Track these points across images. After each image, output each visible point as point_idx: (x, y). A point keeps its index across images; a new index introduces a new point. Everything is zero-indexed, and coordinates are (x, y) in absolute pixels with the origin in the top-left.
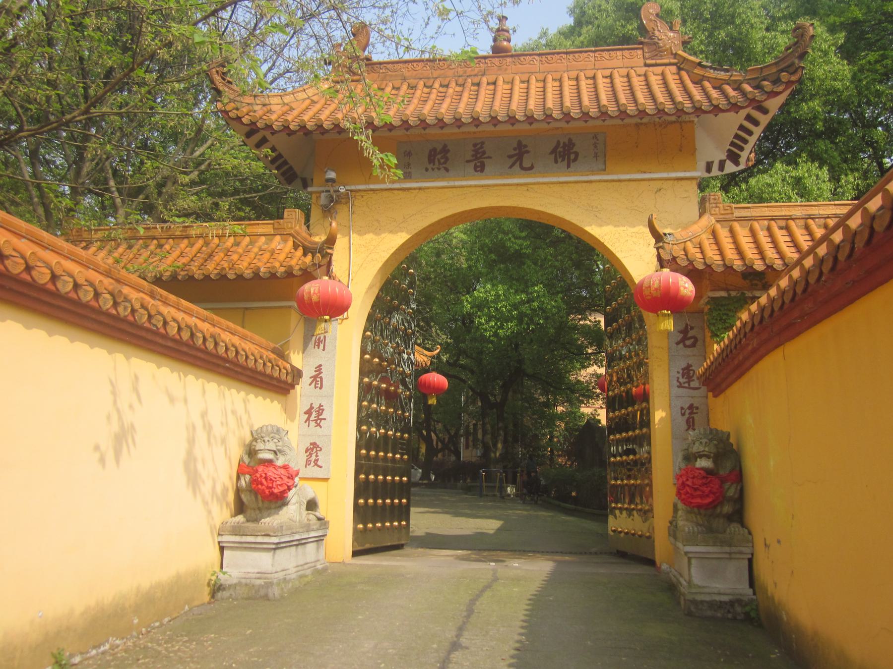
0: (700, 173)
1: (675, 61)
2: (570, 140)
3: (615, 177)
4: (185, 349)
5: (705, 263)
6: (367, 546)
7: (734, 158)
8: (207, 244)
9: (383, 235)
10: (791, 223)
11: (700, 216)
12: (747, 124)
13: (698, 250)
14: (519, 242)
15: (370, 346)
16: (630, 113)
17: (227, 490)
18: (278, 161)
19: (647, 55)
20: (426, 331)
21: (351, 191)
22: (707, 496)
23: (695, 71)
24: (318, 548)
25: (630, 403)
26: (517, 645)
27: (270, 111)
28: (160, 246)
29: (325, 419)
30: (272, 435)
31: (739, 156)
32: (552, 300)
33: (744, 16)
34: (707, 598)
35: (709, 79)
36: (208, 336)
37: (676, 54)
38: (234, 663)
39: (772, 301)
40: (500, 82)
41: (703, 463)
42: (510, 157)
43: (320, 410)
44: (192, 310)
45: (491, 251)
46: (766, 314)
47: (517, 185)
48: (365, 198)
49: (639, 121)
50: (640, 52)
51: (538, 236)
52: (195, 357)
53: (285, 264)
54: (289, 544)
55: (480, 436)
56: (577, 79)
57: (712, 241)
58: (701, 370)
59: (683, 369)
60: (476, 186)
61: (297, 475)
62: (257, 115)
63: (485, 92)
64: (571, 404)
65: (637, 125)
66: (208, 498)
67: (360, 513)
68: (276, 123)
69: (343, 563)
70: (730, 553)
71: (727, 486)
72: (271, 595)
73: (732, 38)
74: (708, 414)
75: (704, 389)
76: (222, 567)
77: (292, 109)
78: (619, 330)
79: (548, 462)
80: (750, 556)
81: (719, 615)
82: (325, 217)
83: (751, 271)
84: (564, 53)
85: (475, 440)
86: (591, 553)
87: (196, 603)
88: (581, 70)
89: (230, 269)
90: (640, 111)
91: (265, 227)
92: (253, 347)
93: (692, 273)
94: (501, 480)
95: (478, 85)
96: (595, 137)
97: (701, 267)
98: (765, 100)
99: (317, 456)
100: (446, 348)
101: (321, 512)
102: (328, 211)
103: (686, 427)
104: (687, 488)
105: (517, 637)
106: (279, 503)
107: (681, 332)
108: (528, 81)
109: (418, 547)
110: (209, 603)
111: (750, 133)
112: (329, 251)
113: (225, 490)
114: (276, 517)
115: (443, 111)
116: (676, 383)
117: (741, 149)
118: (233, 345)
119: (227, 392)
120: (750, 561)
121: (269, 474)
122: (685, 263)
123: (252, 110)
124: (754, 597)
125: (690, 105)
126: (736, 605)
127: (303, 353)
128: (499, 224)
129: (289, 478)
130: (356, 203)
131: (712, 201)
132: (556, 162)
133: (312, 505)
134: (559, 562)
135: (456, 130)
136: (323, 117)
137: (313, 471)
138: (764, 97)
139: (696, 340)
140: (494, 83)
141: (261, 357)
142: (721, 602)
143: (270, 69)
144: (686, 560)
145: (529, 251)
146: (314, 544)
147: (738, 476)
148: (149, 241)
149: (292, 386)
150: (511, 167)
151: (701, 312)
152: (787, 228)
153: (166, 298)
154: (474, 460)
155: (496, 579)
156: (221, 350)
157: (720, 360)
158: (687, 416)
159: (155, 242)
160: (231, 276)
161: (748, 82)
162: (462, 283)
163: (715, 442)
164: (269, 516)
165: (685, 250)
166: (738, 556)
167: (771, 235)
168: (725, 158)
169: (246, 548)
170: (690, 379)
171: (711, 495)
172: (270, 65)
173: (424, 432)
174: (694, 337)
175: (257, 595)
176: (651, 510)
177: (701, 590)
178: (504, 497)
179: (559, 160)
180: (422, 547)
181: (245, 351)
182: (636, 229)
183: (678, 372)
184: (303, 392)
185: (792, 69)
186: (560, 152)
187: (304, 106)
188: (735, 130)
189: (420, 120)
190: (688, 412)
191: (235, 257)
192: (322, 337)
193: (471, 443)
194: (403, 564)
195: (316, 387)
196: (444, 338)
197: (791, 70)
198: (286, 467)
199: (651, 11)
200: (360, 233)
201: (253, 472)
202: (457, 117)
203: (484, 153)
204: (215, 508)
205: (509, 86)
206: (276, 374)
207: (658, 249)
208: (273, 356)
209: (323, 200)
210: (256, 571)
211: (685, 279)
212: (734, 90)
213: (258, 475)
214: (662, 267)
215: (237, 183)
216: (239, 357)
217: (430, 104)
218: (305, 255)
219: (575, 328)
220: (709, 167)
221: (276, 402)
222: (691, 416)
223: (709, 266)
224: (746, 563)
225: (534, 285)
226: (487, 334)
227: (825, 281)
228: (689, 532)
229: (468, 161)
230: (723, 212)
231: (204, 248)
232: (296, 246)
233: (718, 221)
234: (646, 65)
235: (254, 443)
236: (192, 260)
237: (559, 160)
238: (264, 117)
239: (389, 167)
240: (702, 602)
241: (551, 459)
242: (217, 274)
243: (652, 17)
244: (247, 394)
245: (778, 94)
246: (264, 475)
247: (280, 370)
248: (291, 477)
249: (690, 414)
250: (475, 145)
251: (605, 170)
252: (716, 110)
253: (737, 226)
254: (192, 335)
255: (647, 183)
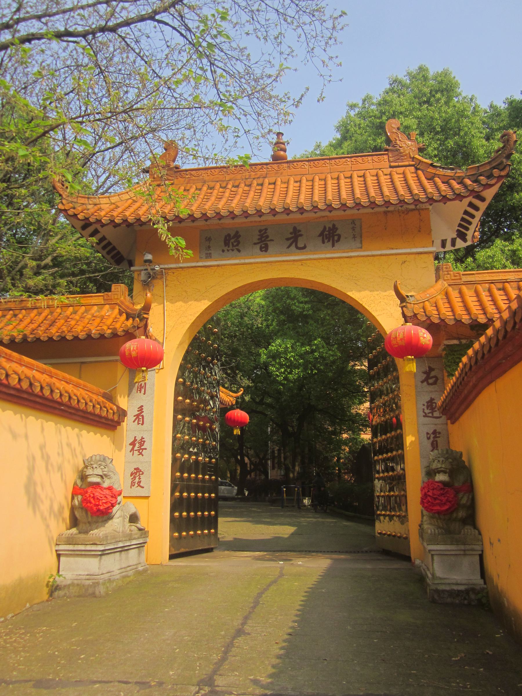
0: (436, 248)
1: (413, 163)
2: (334, 225)
3: (369, 253)
4: (25, 396)
5: (440, 318)
6: (183, 550)
7: (462, 236)
8: (51, 313)
9: (190, 303)
10: (507, 285)
11: (436, 282)
12: (470, 210)
13: (435, 308)
14: (301, 305)
15: (183, 390)
16: (378, 203)
17: (63, 508)
18: (106, 246)
19: (391, 159)
20: (232, 377)
21: (165, 269)
22: (445, 504)
23: (429, 170)
24: (139, 554)
25: (390, 429)
26: (290, 631)
27: (100, 209)
28: (15, 315)
29: (146, 449)
30: (100, 463)
31: (466, 235)
32: (329, 350)
33: (466, 129)
34: (447, 588)
35: (439, 176)
36: (44, 385)
37: (414, 158)
38: (57, 651)
39: (483, 346)
40: (279, 183)
41: (441, 477)
42: (288, 239)
43: (142, 442)
44: (33, 365)
45: (282, 312)
46: (480, 356)
47: (294, 261)
48: (175, 274)
49: (386, 209)
50: (386, 157)
51: (320, 301)
52: (35, 402)
53: (111, 327)
54: (113, 551)
55: (282, 460)
56: (338, 178)
57: (446, 301)
58: (439, 403)
59: (427, 402)
60: (262, 263)
61: (120, 494)
62: (90, 212)
63: (267, 189)
64: (354, 432)
65: (386, 213)
66: (46, 514)
67: (176, 524)
68: (130, 217)
69: (161, 564)
70: (464, 550)
71: (460, 495)
72: (97, 593)
73: (459, 146)
74: (448, 438)
75: (444, 417)
76: (58, 571)
77: (117, 207)
78: (378, 373)
79: (336, 478)
80: (480, 552)
81: (457, 601)
82: (145, 289)
83: (476, 323)
84: (327, 159)
85: (279, 463)
86: (362, 552)
87: (36, 601)
88: (341, 172)
89: (69, 332)
90: (386, 202)
91: (97, 298)
92: (84, 392)
93: (431, 327)
94: (298, 493)
95: (262, 185)
96: (353, 222)
97: (436, 321)
98: (482, 191)
99: (139, 479)
100: (247, 389)
101: (142, 524)
102: (147, 285)
103: (431, 448)
104: (429, 498)
105: (291, 624)
106: (105, 517)
107: (424, 373)
108: (300, 181)
109: (225, 550)
110: (47, 601)
111: (473, 217)
112: (145, 316)
113: (61, 508)
114: (103, 529)
115: (233, 205)
116: (422, 414)
117: (467, 229)
118: (66, 392)
119: (63, 429)
120: (481, 557)
121: (96, 494)
122: (424, 319)
123: (87, 209)
124: (485, 586)
125: (424, 196)
126: (471, 593)
127: (128, 396)
128: (288, 293)
129: (112, 497)
130: (168, 278)
131: (444, 270)
132: (323, 242)
133: (134, 518)
134: (335, 560)
135: (245, 220)
136: (141, 212)
137: (136, 491)
138: (481, 189)
139: (437, 379)
140: (274, 183)
141: (91, 401)
142: (458, 591)
143: (108, 178)
144: (430, 556)
145: (310, 312)
146: (137, 550)
147: (470, 487)
148: (6, 312)
149: (119, 423)
150: (288, 247)
151: (440, 357)
152: (504, 289)
153: (10, 356)
154: (278, 478)
155: (281, 575)
156: (56, 396)
157: (451, 394)
158: (432, 439)
159: (11, 312)
160: (69, 337)
161: (469, 177)
162: (262, 338)
163: (450, 460)
164: (97, 528)
165: (424, 308)
166: (471, 552)
167: (491, 295)
168: (455, 236)
169: (78, 555)
170: (433, 410)
171: (448, 503)
172: (107, 174)
173: (239, 457)
174: (435, 377)
175: (86, 593)
176: (406, 517)
177: (442, 581)
178: (300, 506)
179: (326, 241)
180: (228, 550)
181: (77, 396)
182: (387, 293)
183: (424, 405)
184: (129, 428)
185: (501, 167)
186: (326, 235)
187: (127, 205)
188: (461, 215)
189: (216, 212)
190: (432, 436)
191: (73, 323)
192: (143, 383)
193: (276, 465)
194: (209, 564)
195: (138, 424)
196: (246, 382)
197: (501, 167)
198: (110, 488)
199: (393, 126)
200: (172, 301)
201: (83, 493)
202: (245, 209)
203: (267, 237)
204: (53, 523)
205: (285, 186)
206: (104, 414)
207: (402, 308)
208: (101, 399)
209: (143, 276)
210: (86, 573)
211: (424, 331)
212: (458, 183)
213: (88, 496)
214: (406, 321)
215: (84, 266)
216: (72, 401)
217: (224, 200)
218: (127, 319)
219: (355, 371)
220: (443, 244)
221: (105, 436)
222: (435, 439)
223: (443, 320)
224: (477, 558)
225: (315, 339)
226: (278, 379)
227: (519, 329)
228: (431, 534)
229: (255, 244)
230: (453, 278)
231: (49, 316)
232: (121, 313)
233: (449, 285)
234: (391, 167)
235: (85, 470)
236: (39, 326)
237: (326, 241)
238: (96, 214)
239: (182, 248)
240: (443, 591)
241: (339, 476)
242: (58, 336)
243: (394, 131)
244: (81, 430)
245: (491, 186)
246: (92, 495)
247: (107, 411)
248: (115, 496)
249: (434, 438)
250: (260, 231)
251: (361, 248)
252: (445, 199)
253: (464, 288)
254: (31, 384)
255: (394, 256)
